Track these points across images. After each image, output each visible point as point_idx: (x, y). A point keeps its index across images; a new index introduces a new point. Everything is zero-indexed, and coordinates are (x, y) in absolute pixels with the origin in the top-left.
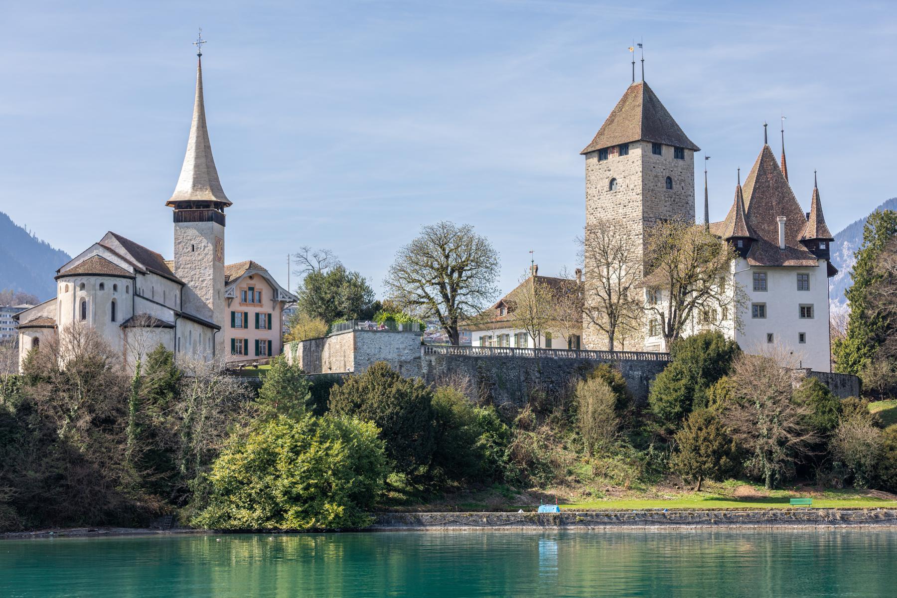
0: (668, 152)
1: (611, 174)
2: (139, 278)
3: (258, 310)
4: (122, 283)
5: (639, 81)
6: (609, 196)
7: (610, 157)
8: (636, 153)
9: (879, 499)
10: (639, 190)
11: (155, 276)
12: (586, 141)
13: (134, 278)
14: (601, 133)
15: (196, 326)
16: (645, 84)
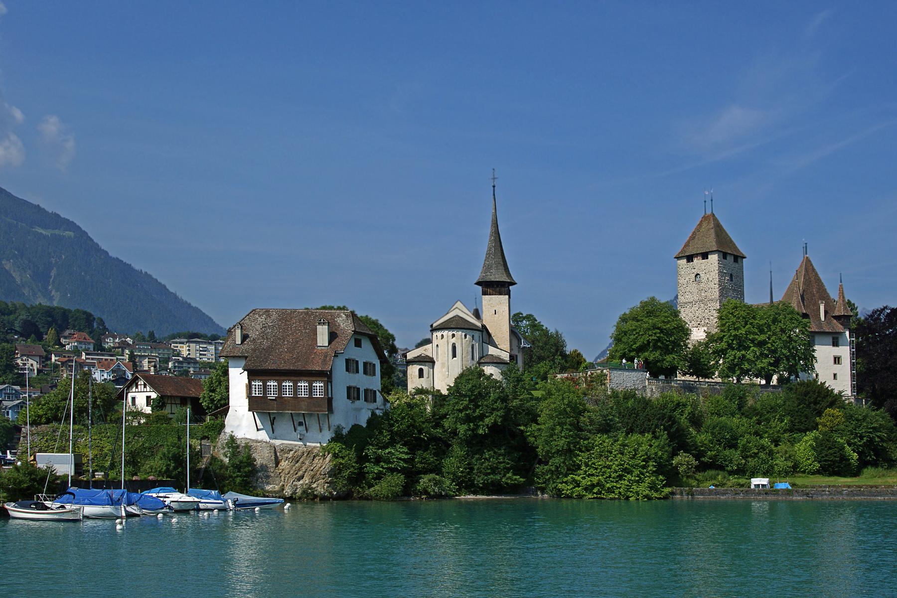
0: (730, 259)
1: (696, 271)
7: (695, 260)
8: (714, 258)
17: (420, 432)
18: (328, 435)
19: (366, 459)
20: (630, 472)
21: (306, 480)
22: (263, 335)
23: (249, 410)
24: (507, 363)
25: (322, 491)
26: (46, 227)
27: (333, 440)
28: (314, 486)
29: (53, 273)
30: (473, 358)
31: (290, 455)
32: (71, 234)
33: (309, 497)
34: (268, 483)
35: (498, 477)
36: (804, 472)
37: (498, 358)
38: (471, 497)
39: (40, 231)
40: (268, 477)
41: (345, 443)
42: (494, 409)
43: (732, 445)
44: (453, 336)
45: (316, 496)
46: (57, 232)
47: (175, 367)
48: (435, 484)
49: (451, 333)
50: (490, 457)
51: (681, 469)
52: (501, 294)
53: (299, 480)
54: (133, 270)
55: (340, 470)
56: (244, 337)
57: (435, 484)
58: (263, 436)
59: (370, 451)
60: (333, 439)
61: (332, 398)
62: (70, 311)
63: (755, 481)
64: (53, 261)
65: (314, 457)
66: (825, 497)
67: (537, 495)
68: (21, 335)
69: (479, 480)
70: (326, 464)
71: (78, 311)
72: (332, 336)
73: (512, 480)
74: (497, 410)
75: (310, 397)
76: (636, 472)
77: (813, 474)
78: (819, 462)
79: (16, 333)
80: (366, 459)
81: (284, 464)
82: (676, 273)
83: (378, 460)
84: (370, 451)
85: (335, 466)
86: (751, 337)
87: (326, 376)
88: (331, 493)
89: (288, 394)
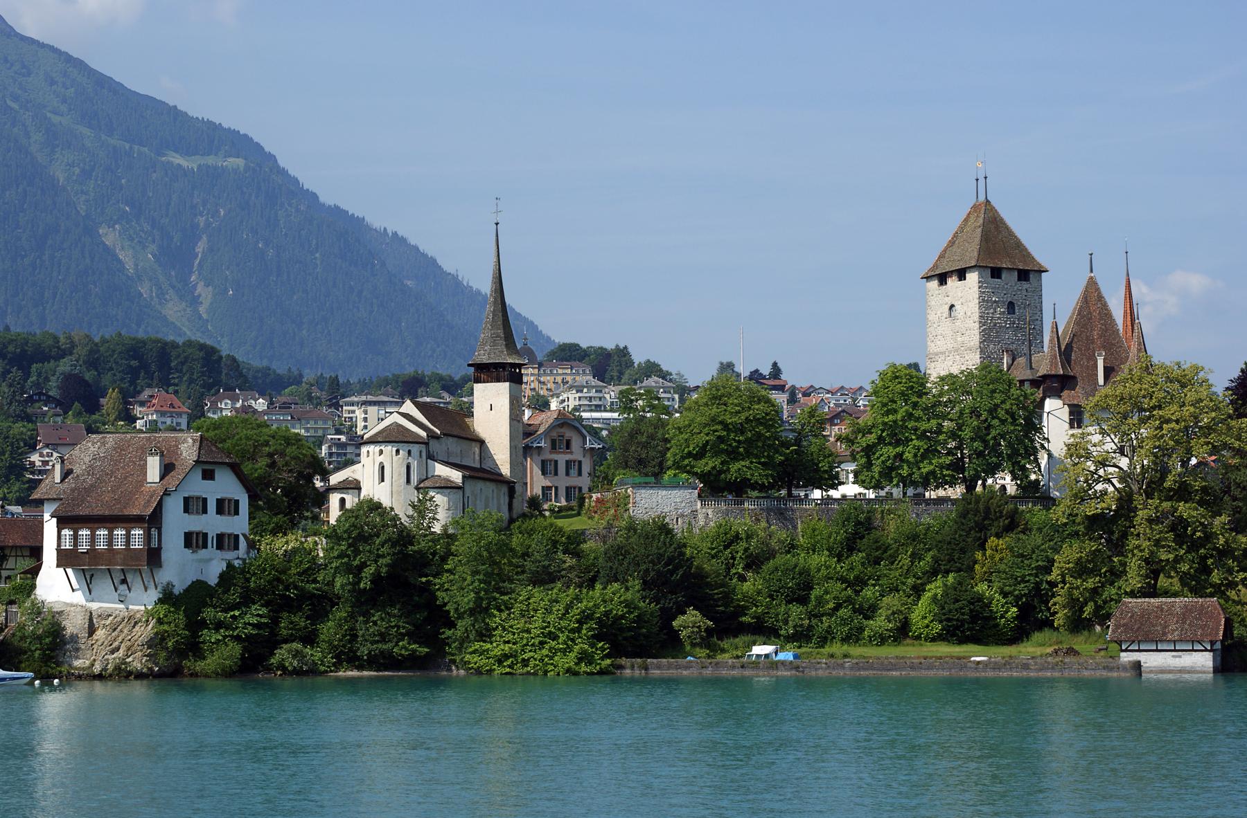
0: (1010, 279)
1: (949, 301)
2: (432, 443)
3: (568, 457)
4: (415, 449)
5: (982, 198)
6: (948, 322)
7: (949, 281)
8: (973, 277)
9: (1182, 671)
10: (976, 317)
11: (451, 439)
12: (926, 267)
13: (427, 444)
14: (942, 256)
15: (488, 483)
16: (988, 201)
17: (287, 588)
18: (153, 595)
19: (203, 624)
20: (554, 637)
21: (121, 653)
22: (90, 470)
23: (58, 566)
24: (459, 488)
25: (139, 666)
26: (187, 153)
27: (161, 601)
28: (130, 659)
29: (200, 248)
30: (408, 481)
31: (108, 622)
32: (240, 162)
33: (122, 674)
34: (77, 658)
35: (390, 645)
36: (918, 638)
37: (447, 480)
38: (355, 673)
39: (178, 160)
40: (78, 650)
41: (174, 605)
42: (379, 556)
43: (801, 599)
44: (381, 452)
45: (130, 673)
46: (210, 160)
47: (331, 454)
48: (294, 657)
49: (377, 448)
50: (379, 621)
51: (683, 634)
52: (498, 381)
53: (112, 652)
54: (369, 228)
55: (163, 639)
56: (66, 474)
57: (294, 657)
58: (79, 598)
59: (209, 614)
60: (160, 600)
61: (159, 549)
62: (174, 345)
63: (759, 650)
64: (201, 221)
65: (136, 623)
66: (820, 672)
67: (450, 670)
68: (58, 403)
69: (364, 651)
70: (144, 632)
71: (189, 344)
72: (167, 469)
73: (407, 649)
74: (383, 556)
75: (128, 549)
76: (562, 637)
77: (933, 640)
78: (941, 622)
79: (49, 400)
80: (203, 624)
81: (100, 634)
82: (923, 305)
83: (219, 625)
84: (209, 614)
85: (156, 634)
86: (911, 424)
87: (153, 521)
88: (151, 669)
89: (101, 546)
